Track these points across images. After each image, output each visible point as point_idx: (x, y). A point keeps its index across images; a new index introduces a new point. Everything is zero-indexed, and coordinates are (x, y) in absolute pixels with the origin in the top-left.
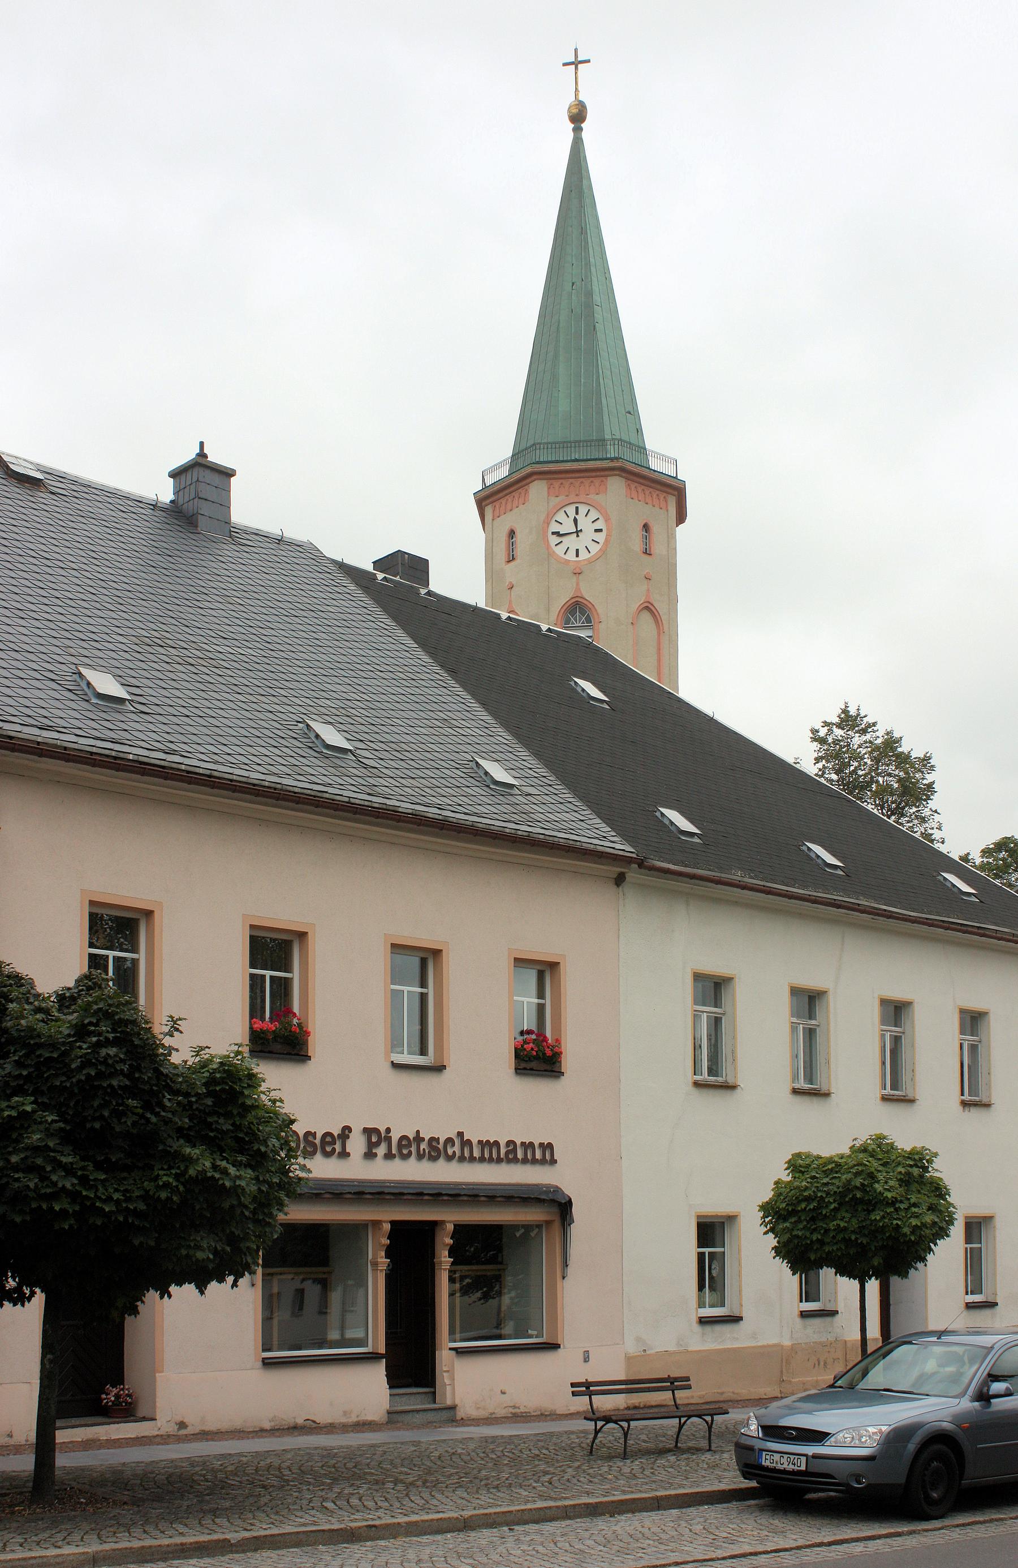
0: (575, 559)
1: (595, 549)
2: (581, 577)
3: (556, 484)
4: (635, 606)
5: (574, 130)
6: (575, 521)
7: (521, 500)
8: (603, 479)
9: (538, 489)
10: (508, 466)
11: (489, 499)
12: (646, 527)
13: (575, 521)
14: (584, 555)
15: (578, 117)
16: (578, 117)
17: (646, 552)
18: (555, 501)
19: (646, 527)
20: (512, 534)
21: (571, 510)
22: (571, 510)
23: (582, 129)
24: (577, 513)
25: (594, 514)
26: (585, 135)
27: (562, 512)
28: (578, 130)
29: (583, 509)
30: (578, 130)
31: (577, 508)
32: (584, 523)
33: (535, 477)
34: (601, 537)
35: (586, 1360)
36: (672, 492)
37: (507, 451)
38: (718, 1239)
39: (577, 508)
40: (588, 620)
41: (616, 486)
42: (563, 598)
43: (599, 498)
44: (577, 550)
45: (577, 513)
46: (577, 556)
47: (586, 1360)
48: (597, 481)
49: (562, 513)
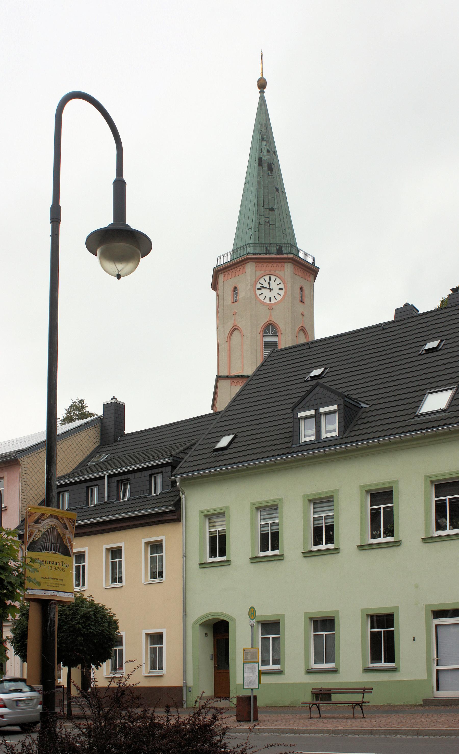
0: (269, 302)
1: (279, 298)
2: (272, 311)
3: (260, 264)
4: (297, 329)
5: (260, 92)
6: (269, 283)
7: (241, 272)
8: (244, 266)
9: (250, 268)
10: (230, 256)
11: (219, 272)
12: (301, 289)
13: (269, 283)
14: (273, 301)
15: (262, 85)
16: (262, 85)
17: (302, 302)
18: (259, 273)
19: (301, 289)
20: (235, 289)
21: (267, 278)
22: (267, 278)
23: (264, 92)
24: (270, 280)
25: (278, 281)
26: (265, 95)
27: (262, 279)
28: (262, 92)
29: (273, 278)
30: (262, 92)
31: (270, 277)
32: (274, 285)
33: (290, 261)
34: (282, 293)
35: (414, 640)
36: (311, 271)
37: (230, 248)
38: (373, 662)
39: (270, 277)
40: (275, 333)
41: (288, 268)
42: (262, 322)
43: (281, 273)
44: (270, 298)
45: (270, 280)
46: (270, 301)
47: (414, 640)
48: (280, 264)
49: (262, 279)
